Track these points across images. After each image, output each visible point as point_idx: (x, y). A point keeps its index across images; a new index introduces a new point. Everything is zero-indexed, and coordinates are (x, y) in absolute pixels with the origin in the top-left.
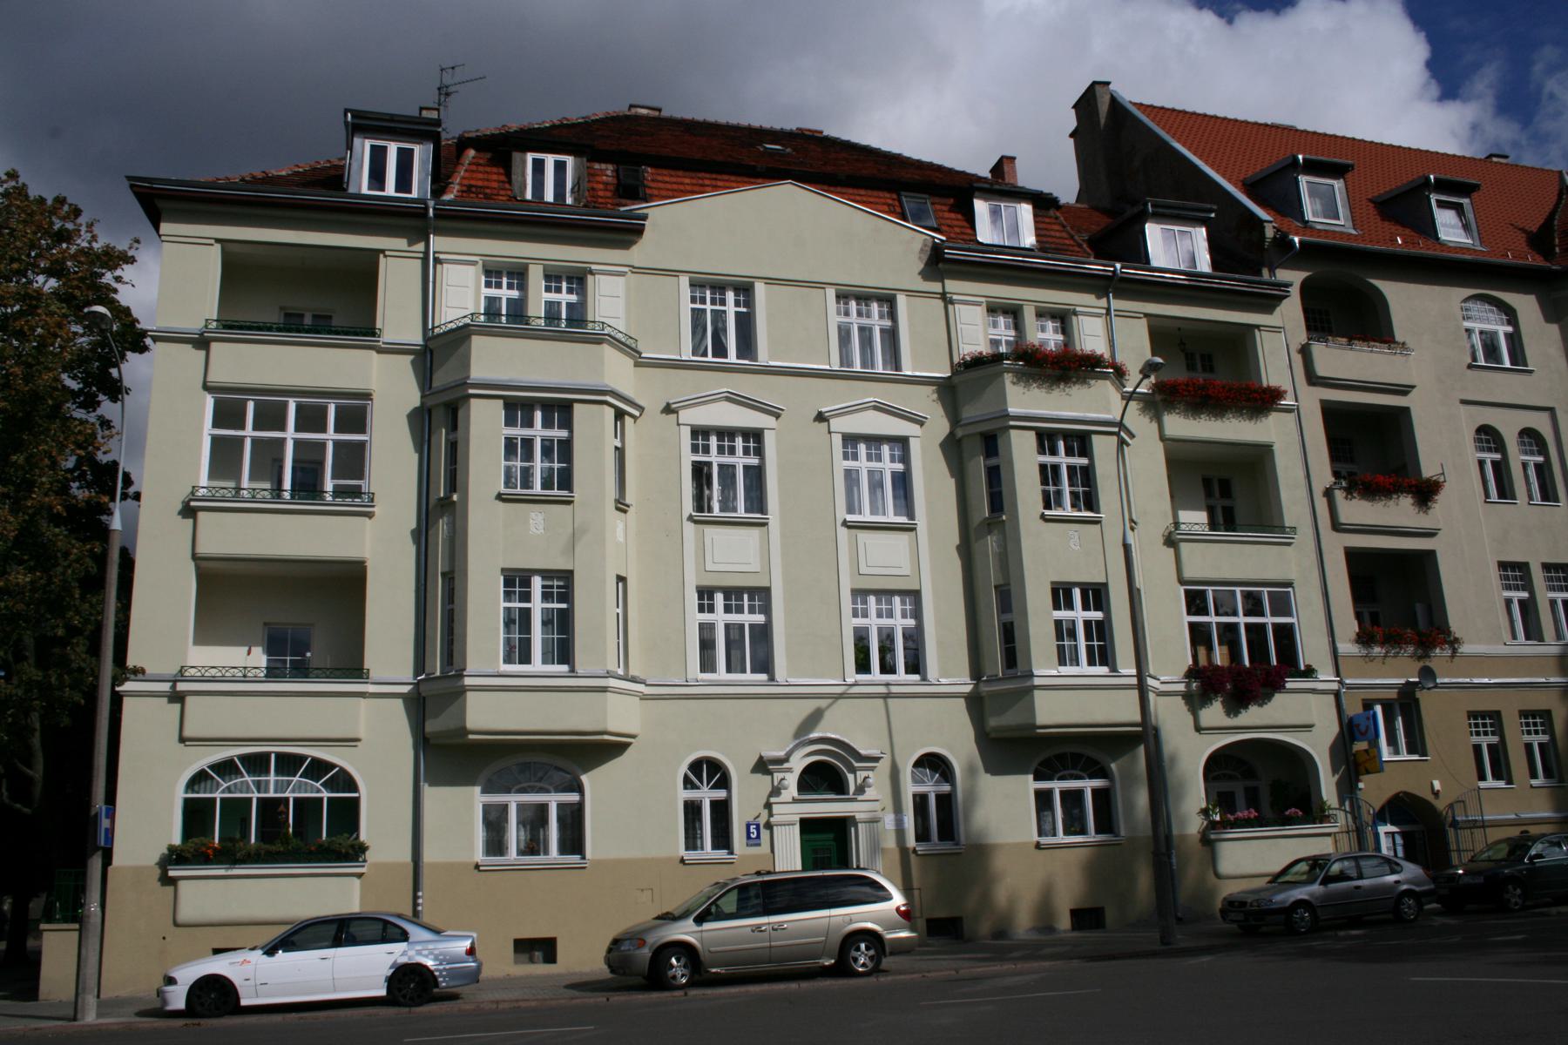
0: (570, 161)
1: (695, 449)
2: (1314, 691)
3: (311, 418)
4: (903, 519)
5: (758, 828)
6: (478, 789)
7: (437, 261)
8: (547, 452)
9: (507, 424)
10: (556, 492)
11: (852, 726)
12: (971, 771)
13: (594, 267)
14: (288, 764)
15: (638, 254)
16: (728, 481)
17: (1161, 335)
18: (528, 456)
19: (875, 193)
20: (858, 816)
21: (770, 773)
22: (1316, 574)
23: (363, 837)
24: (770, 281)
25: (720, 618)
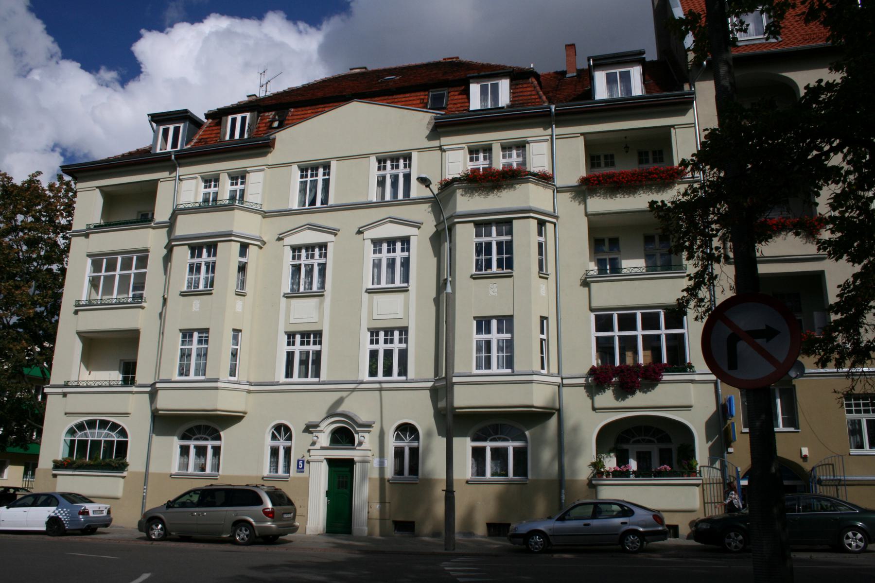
2: (692, 381)
5: (303, 463)
6: (468, 439)
7: (180, 179)
9: (477, 236)
10: (505, 271)
11: (360, 407)
12: (429, 435)
13: (529, 139)
14: (104, 424)
15: (272, 158)
16: (308, 273)
19: (413, 94)
20: (356, 459)
21: (311, 433)
23: (128, 460)
24: (339, 159)
25: (297, 348)
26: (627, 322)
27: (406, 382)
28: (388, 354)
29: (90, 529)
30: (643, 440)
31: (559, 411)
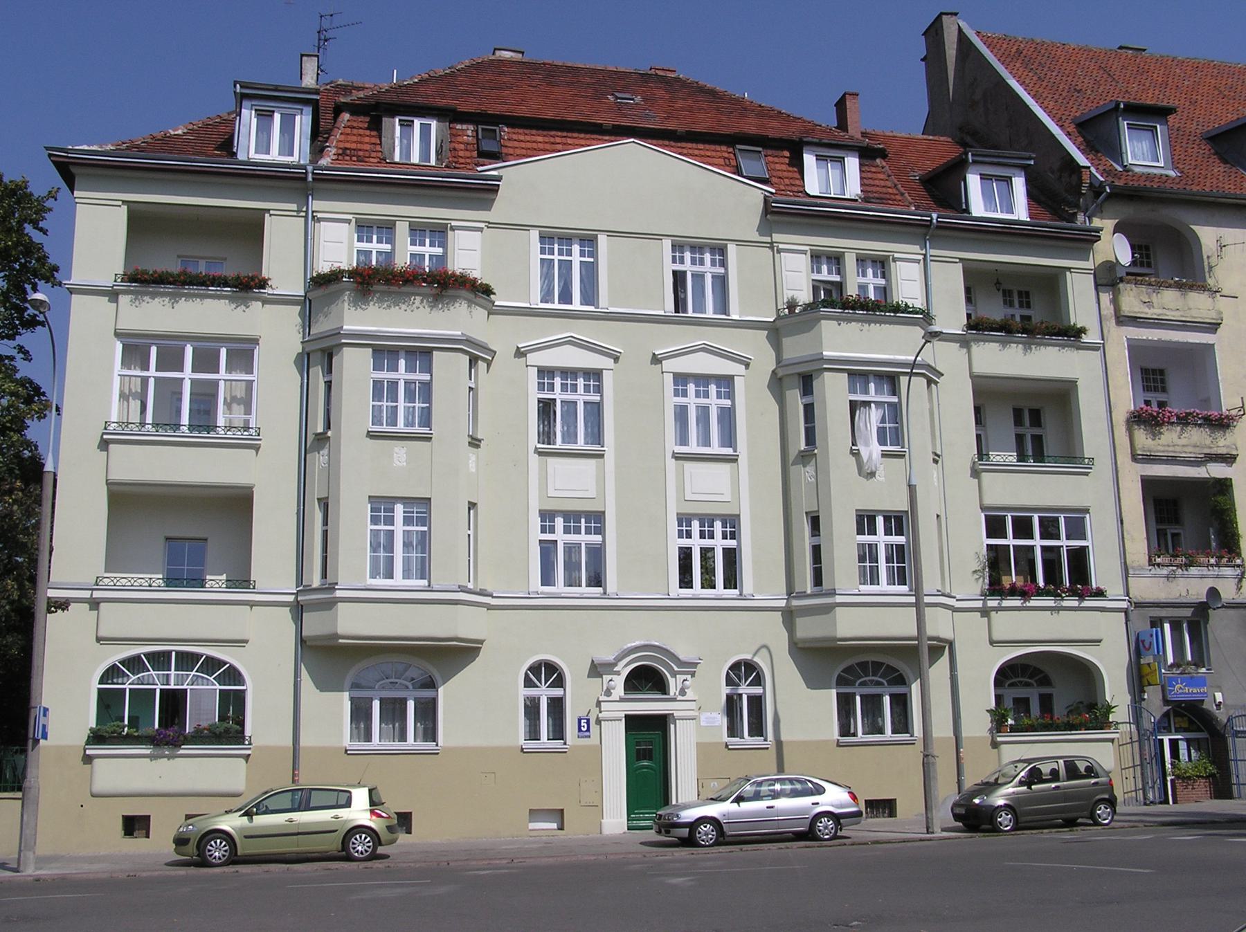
0: (434, 124)
1: (541, 387)
3: (206, 361)
4: (729, 451)
8: (410, 396)
14: (187, 661)
15: (493, 215)
17: (977, 282)
18: (394, 397)
20: (676, 714)
22: (1112, 500)
24: (611, 233)
25: (560, 536)
26: (1023, 528)
27: (429, 589)
28: (706, 553)
29: (343, 847)
30: (872, 681)
31: (951, 644)
